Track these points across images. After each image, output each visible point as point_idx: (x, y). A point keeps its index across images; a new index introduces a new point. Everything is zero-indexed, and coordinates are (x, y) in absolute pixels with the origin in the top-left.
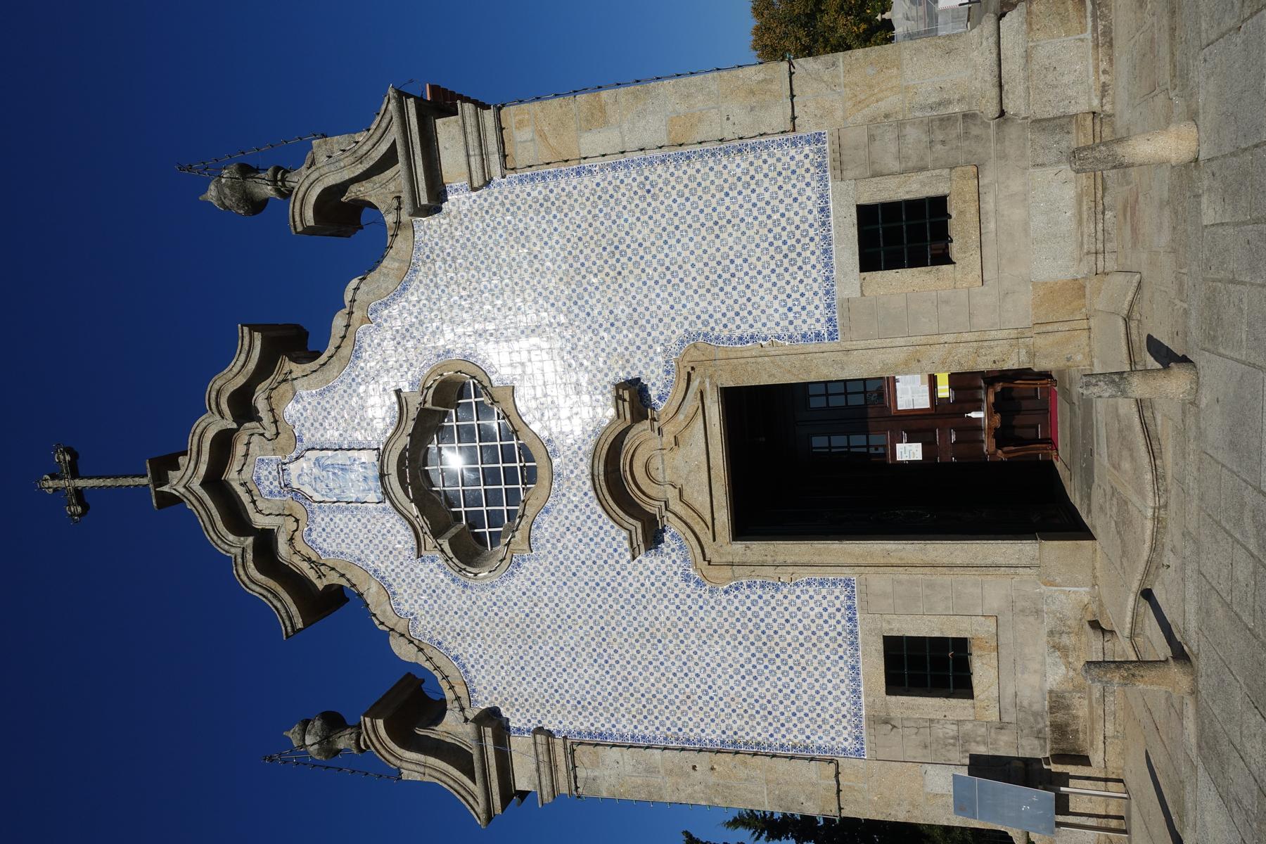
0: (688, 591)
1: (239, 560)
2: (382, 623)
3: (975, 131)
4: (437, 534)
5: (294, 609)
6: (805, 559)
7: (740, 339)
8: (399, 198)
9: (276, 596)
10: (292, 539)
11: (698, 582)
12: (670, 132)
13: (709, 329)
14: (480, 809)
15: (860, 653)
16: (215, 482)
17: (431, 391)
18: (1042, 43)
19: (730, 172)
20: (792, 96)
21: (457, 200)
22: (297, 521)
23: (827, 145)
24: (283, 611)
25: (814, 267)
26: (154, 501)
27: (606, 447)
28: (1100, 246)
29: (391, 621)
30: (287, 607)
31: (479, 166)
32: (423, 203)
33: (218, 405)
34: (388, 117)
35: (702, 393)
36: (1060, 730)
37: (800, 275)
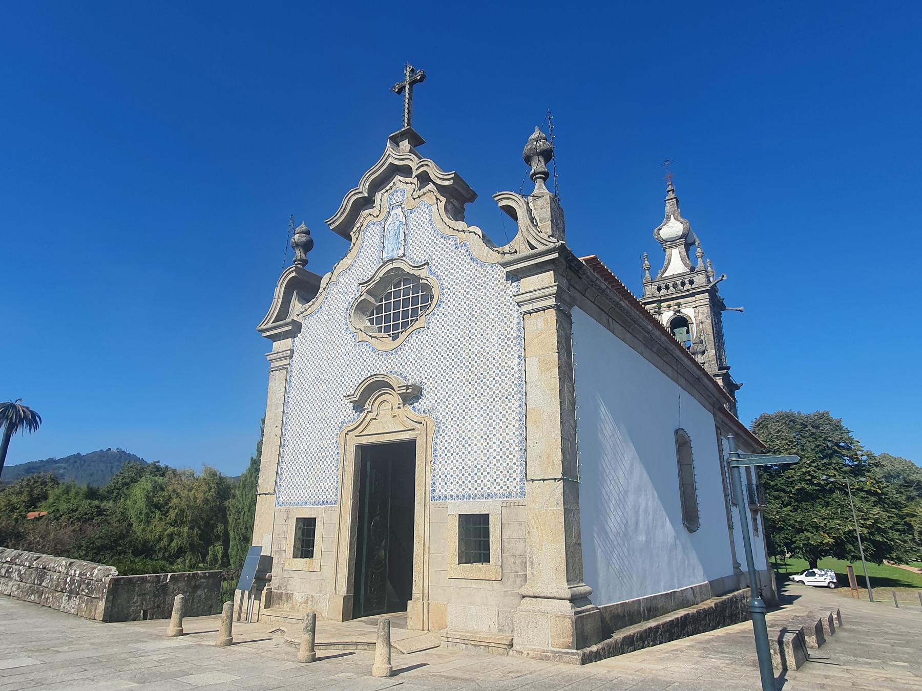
0: (338, 423)
1: (357, 191)
2: (335, 268)
3: (518, 580)
4: (369, 292)
5: (337, 223)
6: (345, 481)
7: (436, 450)
8: (516, 252)
9: (342, 213)
10: (370, 215)
11: (341, 428)
12: (533, 409)
13: (441, 433)
14: (263, 327)
15: (311, 506)
16: (394, 170)
17: (426, 282)
18: (549, 622)
19: (512, 444)
20: (544, 480)
21: (512, 288)
22: (377, 216)
23: (519, 499)
24: (336, 218)
25: (464, 489)
26: (392, 135)
27: (388, 381)
28: (450, 640)
29: (336, 272)
30: (339, 219)
31: (525, 299)
32: (558, 256)
33: (422, 166)
34: (547, 243)
35: (414, 429)
36: (280, 597)
37: (460, 482)
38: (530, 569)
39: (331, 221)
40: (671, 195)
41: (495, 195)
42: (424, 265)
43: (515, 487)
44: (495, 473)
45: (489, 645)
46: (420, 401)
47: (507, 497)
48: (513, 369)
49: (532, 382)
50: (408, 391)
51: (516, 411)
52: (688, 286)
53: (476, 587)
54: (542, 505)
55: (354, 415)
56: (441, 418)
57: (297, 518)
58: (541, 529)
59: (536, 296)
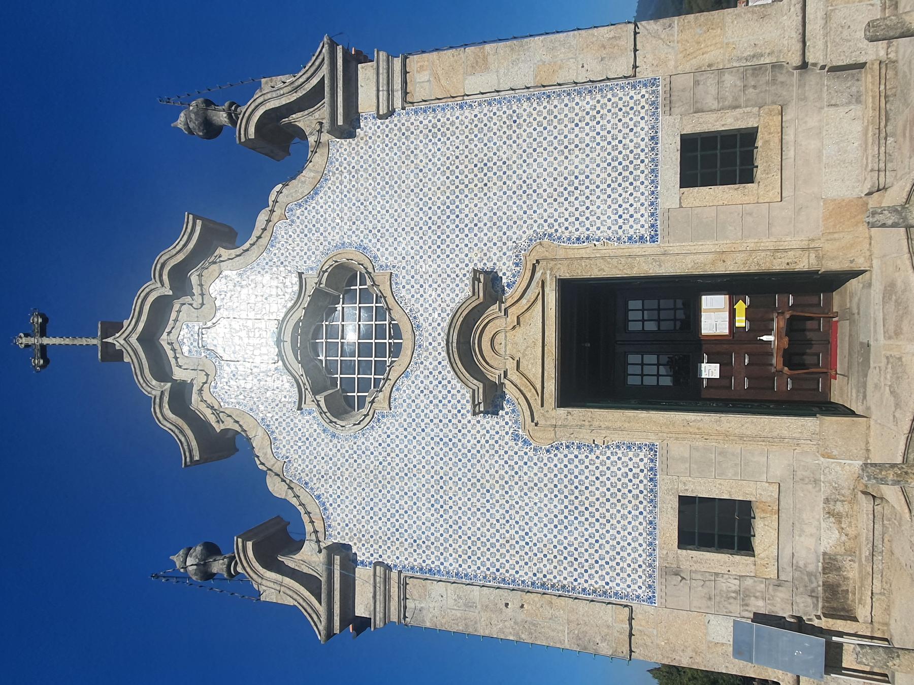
0: (516, 449)
1: (158, 400)
2: (263, 464)
4: (315, 392)
5: (194, 444)
7: (578, 239)
9: (182, 431)
12: (536, 76)
13: (553, 230)
18: (839, 7)
20: (635, 50)
21: (368, 126)
23: (660, 88)
24: (185, 444)
25: (642, 183)
28: (882, 165)
33: (161, 275)
34: (321, 57)
35: (543, 283)
38: (762, 59)
39: (187, 454)
41: (237, 139)
43: (643, 96)
44: (620, 131)
45: (883, 94)
46: (500, 274)
47: (657, 108)
48: (476, 116)
49: (499, 82)
50: (482, 280)
51: (535, 105)
53: (793, 149)
54: (670, 50)
55: (507, 413)
56: (531, 232)
57: (679, 548)
58: (705, 47)
59: (385, 82)
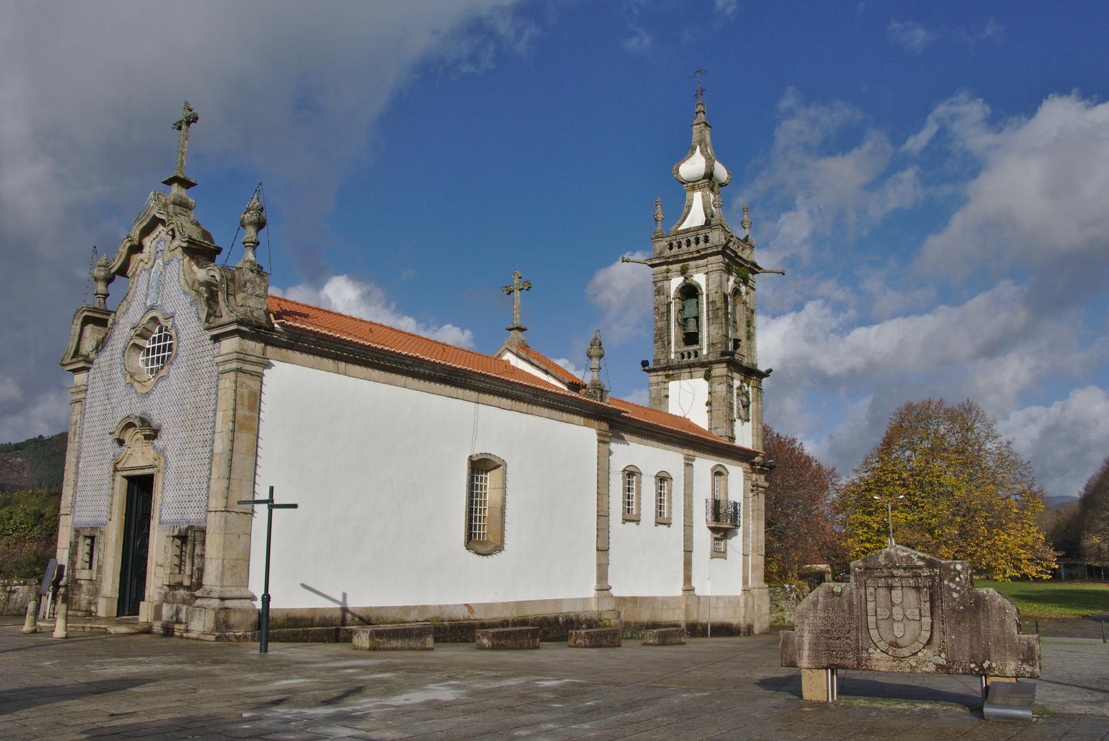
40: (702, 117)
42: (170, 318)
52: (702, 245)
